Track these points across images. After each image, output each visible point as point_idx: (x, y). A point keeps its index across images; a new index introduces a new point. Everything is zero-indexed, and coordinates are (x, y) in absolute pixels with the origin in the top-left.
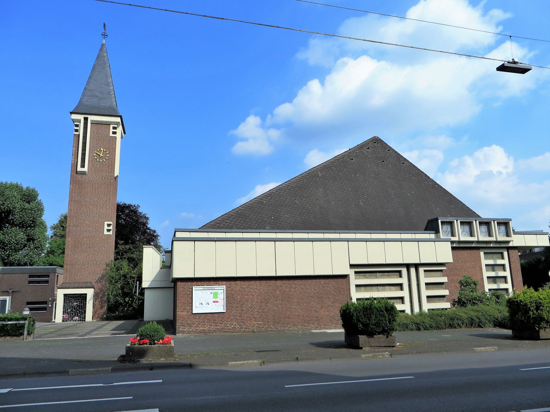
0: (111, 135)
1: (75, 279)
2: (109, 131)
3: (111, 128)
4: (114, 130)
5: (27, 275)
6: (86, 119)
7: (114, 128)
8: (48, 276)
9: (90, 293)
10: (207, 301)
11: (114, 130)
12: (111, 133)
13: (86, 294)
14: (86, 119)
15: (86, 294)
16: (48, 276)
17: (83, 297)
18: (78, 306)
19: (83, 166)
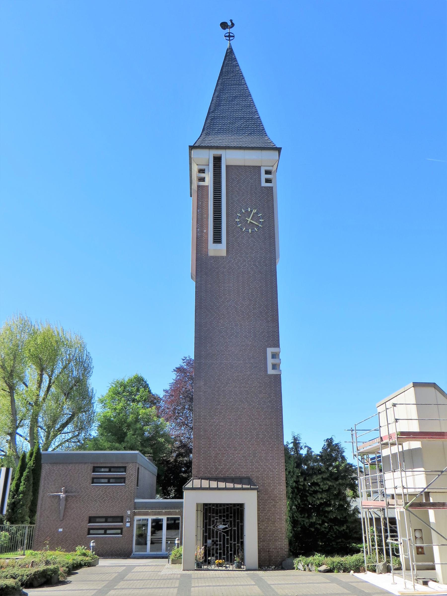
0: (264, 184)
1: (217, 469)
2: (266, 364)
3: (263, 172)
4: (269, 176)
5: (90, 467)
6: (217, 160)
7: (268, 172)
8: (124, 469)
9: (249, 499)
10: (357, 482)
11: (269, 176)
12: (263, 181)
13: (241, 506)
14: (217, 160)
15: (241, 506)
16: (124, 469)
17: (235, 512)
18: (227, 532)
19: (217, 239)
